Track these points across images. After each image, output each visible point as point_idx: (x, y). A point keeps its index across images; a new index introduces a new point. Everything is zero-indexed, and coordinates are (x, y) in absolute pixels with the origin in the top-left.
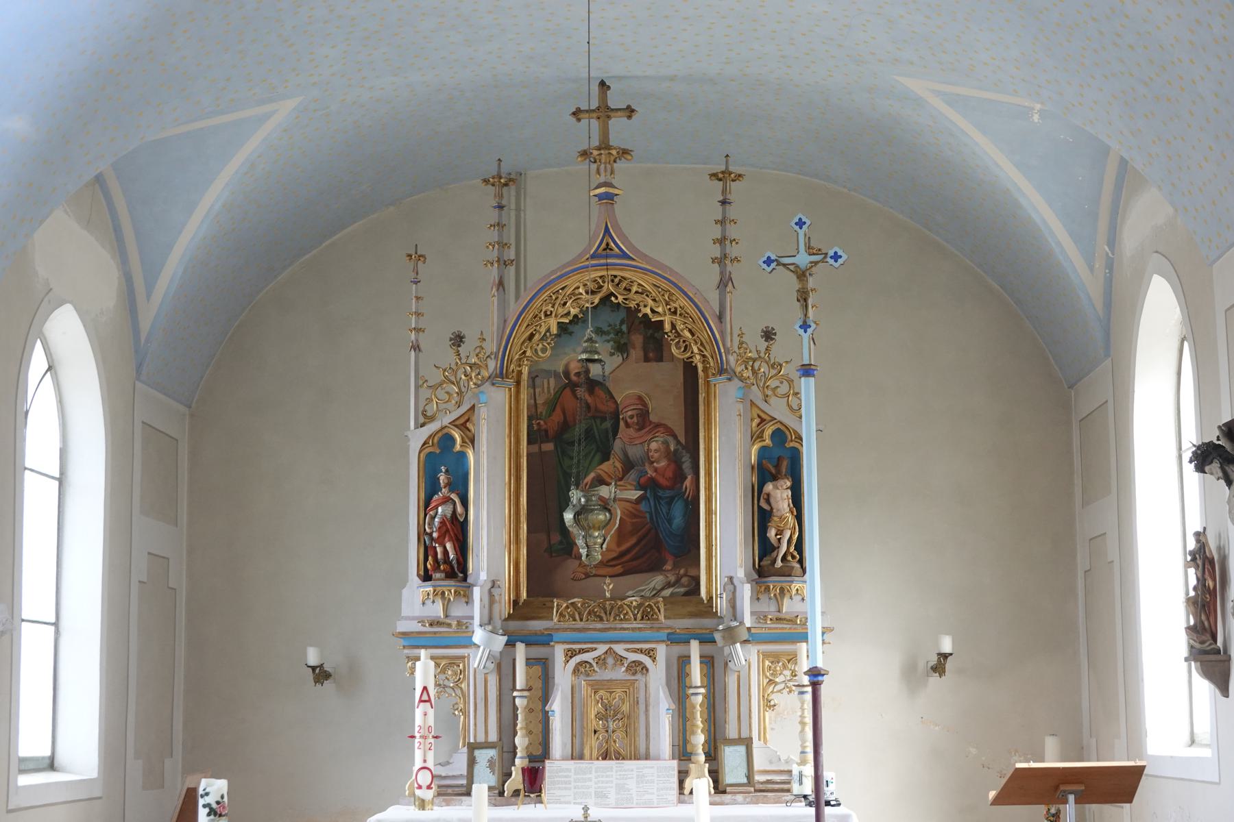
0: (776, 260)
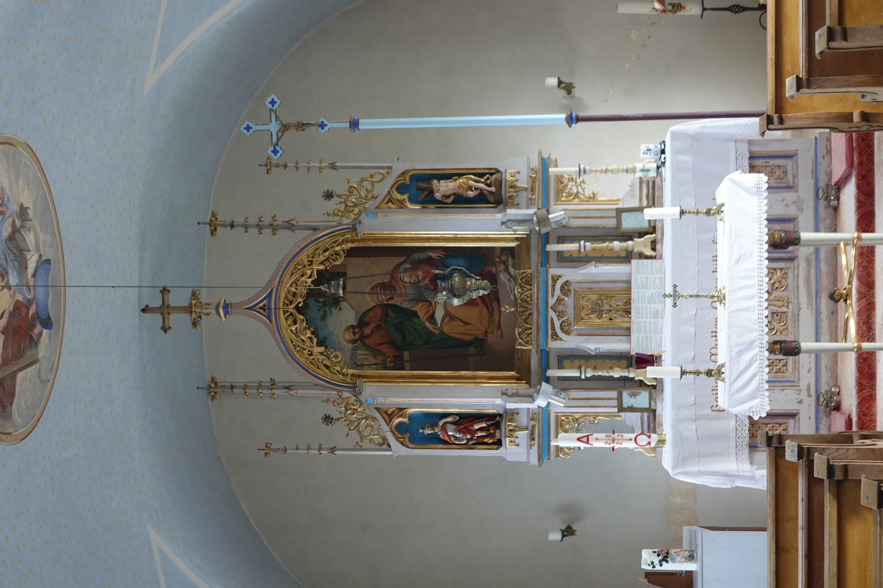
0: (274, 146)
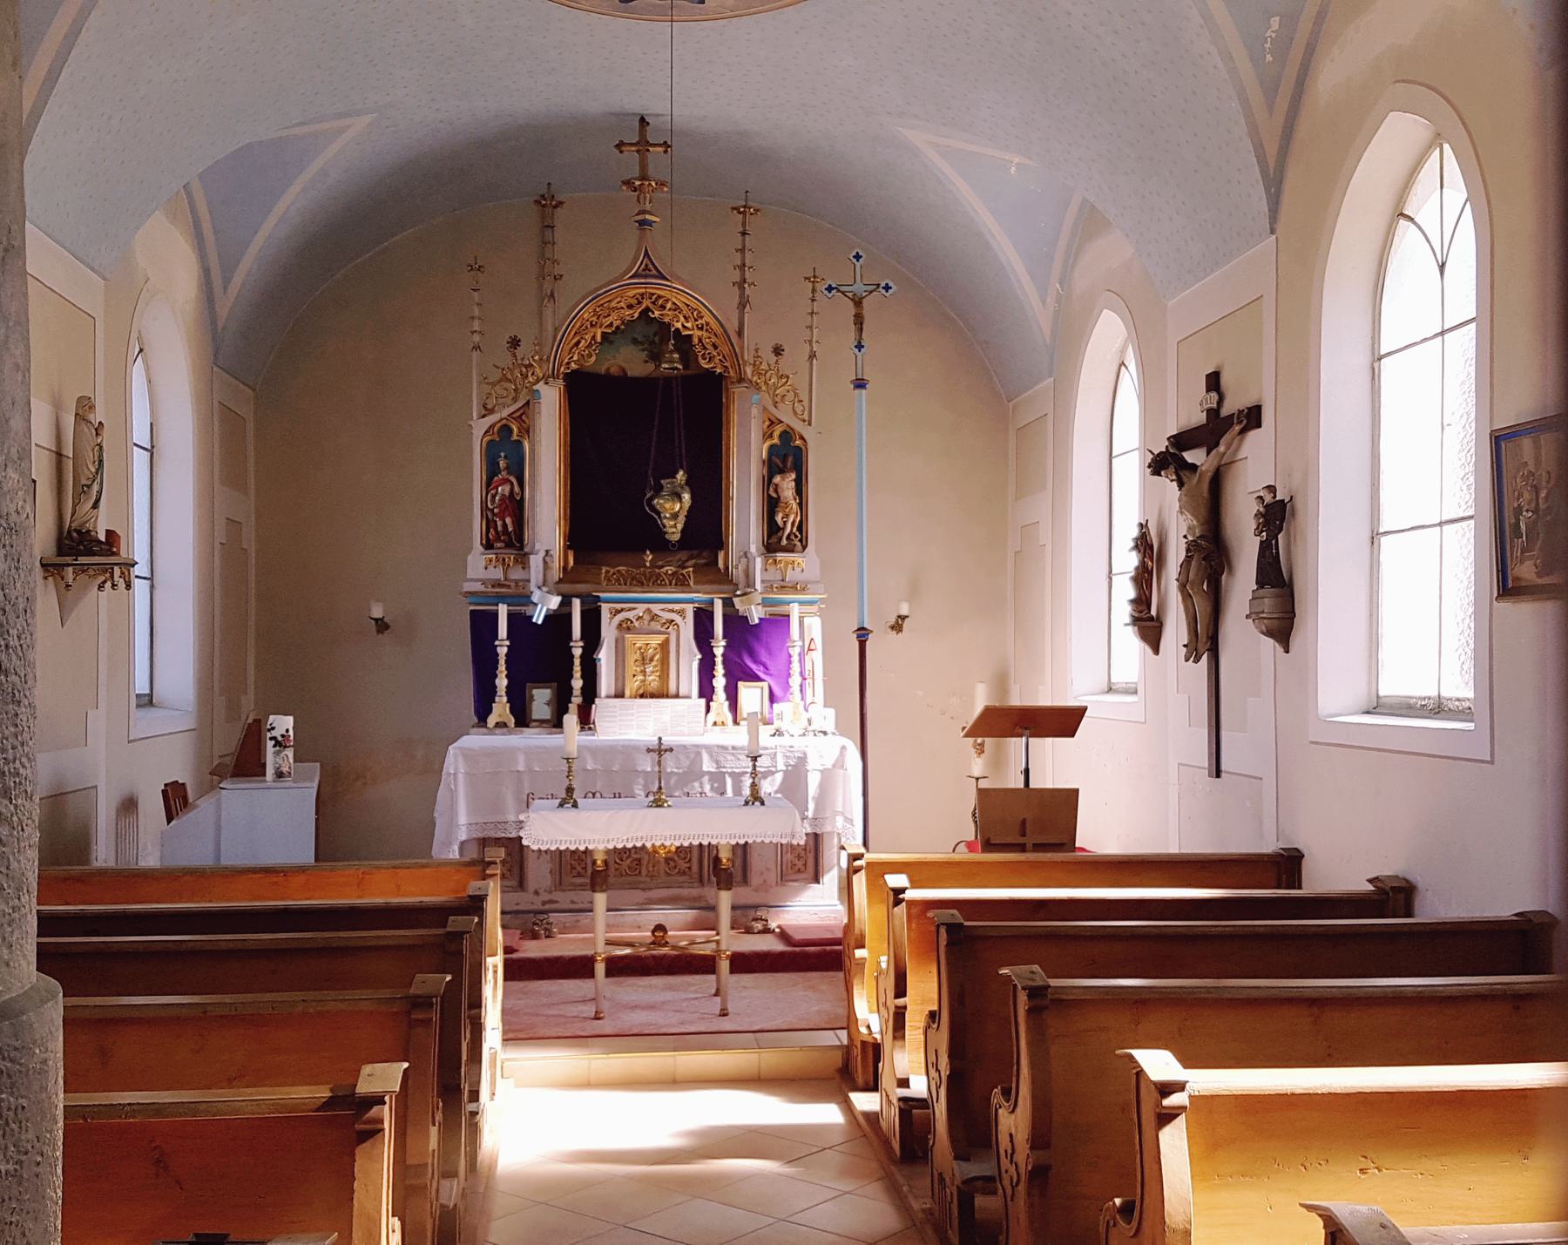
0: (836, 288)
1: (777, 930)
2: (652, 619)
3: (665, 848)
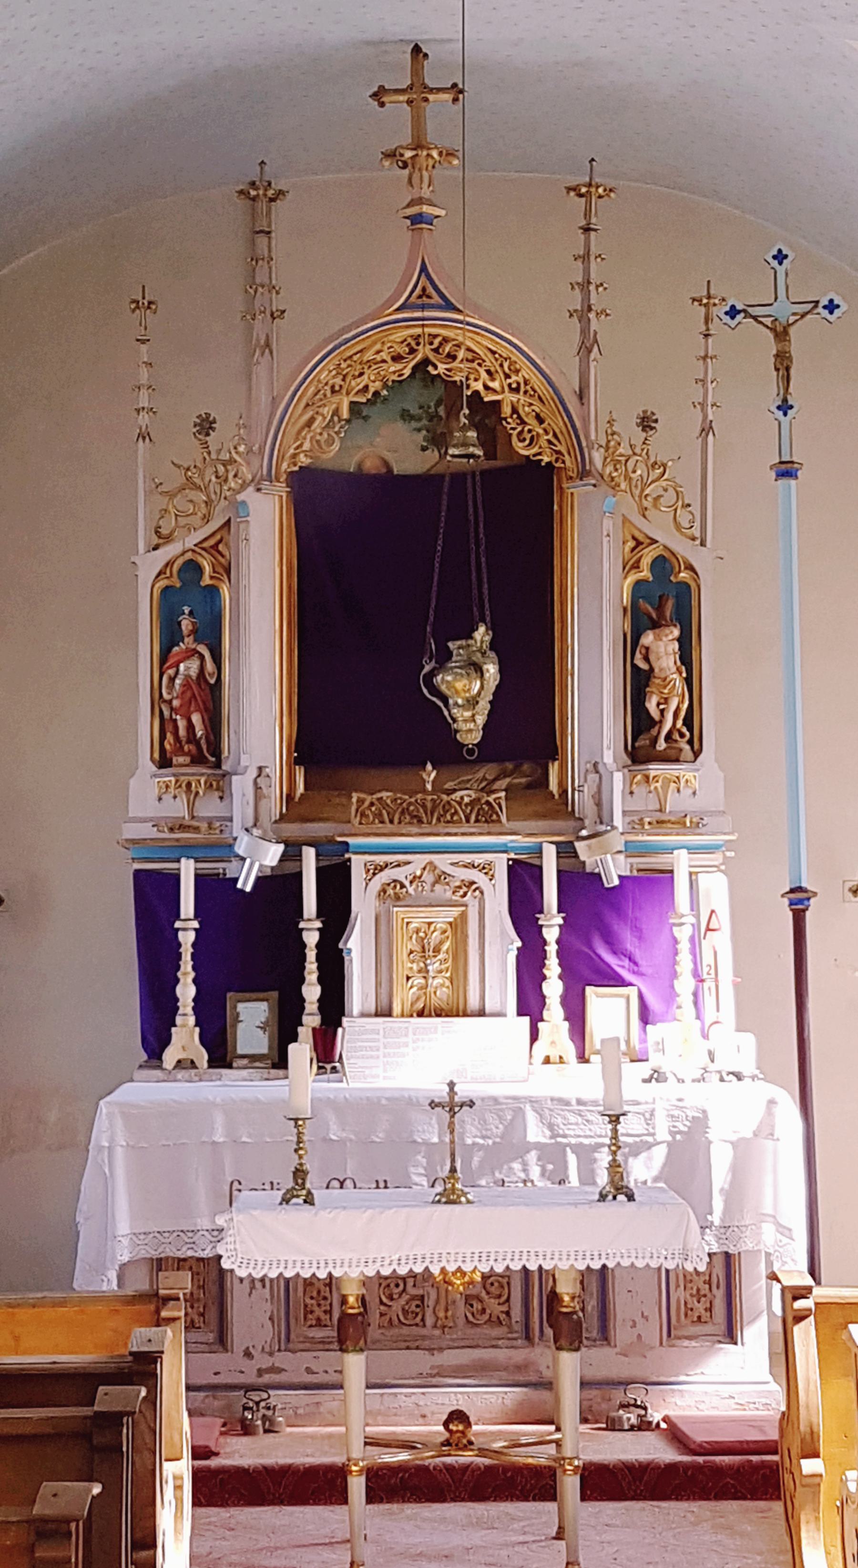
0: (744, 311)
1: (663, 1425)
2: (437, 881)
3: (464, 1274)
